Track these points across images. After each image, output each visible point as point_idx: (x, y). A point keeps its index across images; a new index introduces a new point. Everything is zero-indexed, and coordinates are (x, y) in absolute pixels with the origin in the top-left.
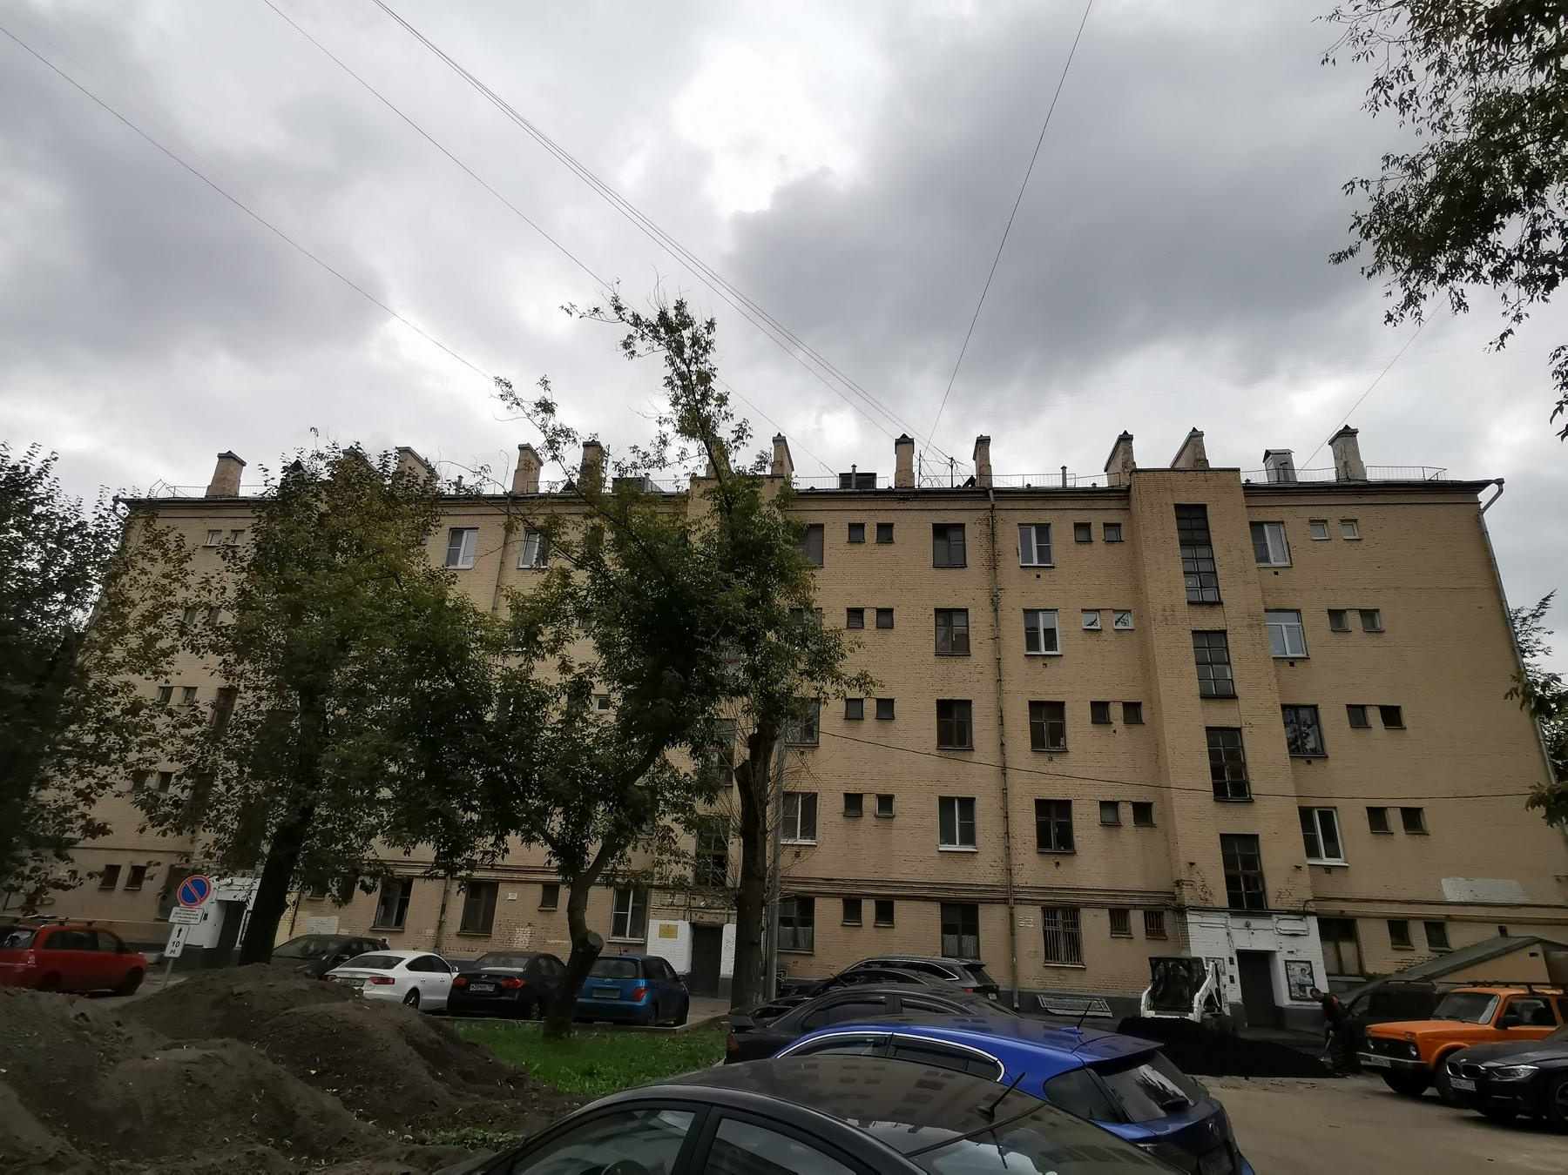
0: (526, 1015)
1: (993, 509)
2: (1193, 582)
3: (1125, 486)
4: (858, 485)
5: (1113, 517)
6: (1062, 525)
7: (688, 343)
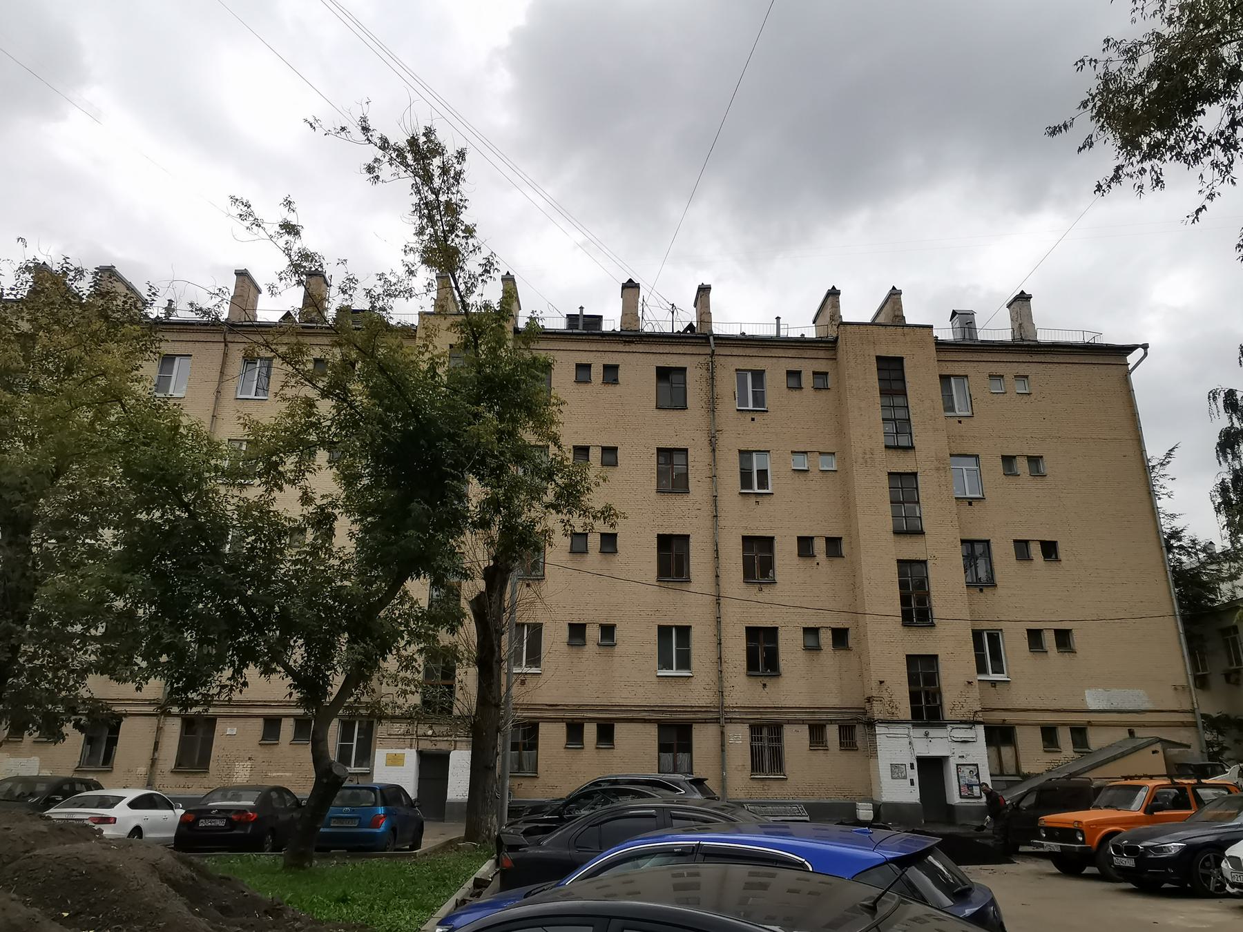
0: (259, 848)
1: (713, 354)
2: (890, 427)
3: (831, 339)
4: (584, 327)
5: (821, 366)
6: (775, 370)
7: (437, 172)
